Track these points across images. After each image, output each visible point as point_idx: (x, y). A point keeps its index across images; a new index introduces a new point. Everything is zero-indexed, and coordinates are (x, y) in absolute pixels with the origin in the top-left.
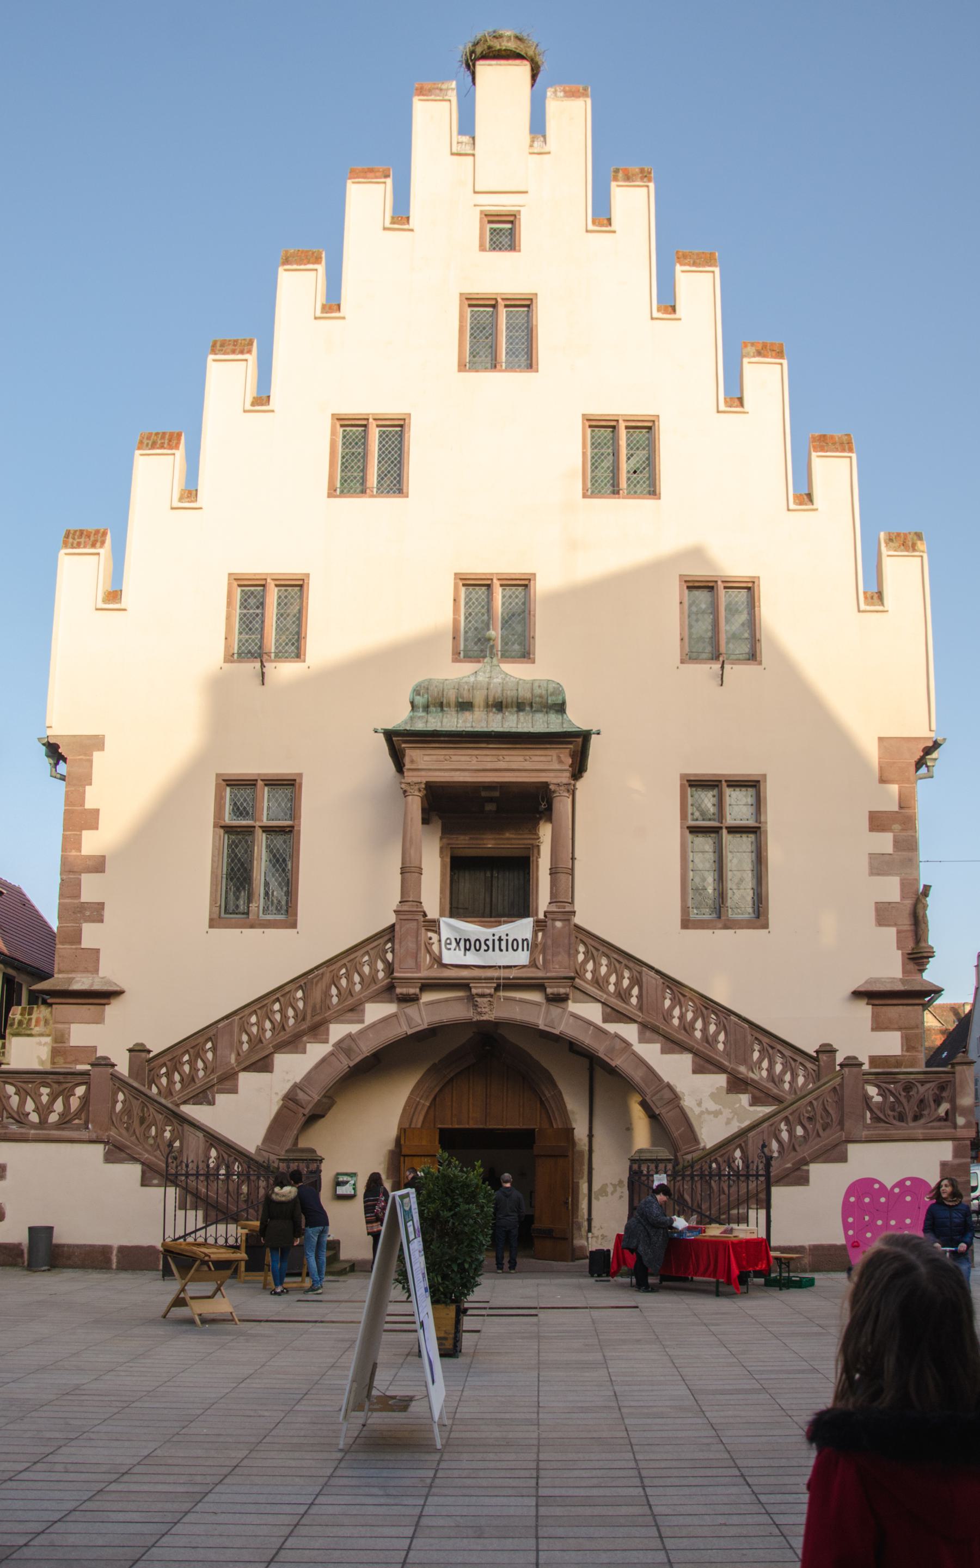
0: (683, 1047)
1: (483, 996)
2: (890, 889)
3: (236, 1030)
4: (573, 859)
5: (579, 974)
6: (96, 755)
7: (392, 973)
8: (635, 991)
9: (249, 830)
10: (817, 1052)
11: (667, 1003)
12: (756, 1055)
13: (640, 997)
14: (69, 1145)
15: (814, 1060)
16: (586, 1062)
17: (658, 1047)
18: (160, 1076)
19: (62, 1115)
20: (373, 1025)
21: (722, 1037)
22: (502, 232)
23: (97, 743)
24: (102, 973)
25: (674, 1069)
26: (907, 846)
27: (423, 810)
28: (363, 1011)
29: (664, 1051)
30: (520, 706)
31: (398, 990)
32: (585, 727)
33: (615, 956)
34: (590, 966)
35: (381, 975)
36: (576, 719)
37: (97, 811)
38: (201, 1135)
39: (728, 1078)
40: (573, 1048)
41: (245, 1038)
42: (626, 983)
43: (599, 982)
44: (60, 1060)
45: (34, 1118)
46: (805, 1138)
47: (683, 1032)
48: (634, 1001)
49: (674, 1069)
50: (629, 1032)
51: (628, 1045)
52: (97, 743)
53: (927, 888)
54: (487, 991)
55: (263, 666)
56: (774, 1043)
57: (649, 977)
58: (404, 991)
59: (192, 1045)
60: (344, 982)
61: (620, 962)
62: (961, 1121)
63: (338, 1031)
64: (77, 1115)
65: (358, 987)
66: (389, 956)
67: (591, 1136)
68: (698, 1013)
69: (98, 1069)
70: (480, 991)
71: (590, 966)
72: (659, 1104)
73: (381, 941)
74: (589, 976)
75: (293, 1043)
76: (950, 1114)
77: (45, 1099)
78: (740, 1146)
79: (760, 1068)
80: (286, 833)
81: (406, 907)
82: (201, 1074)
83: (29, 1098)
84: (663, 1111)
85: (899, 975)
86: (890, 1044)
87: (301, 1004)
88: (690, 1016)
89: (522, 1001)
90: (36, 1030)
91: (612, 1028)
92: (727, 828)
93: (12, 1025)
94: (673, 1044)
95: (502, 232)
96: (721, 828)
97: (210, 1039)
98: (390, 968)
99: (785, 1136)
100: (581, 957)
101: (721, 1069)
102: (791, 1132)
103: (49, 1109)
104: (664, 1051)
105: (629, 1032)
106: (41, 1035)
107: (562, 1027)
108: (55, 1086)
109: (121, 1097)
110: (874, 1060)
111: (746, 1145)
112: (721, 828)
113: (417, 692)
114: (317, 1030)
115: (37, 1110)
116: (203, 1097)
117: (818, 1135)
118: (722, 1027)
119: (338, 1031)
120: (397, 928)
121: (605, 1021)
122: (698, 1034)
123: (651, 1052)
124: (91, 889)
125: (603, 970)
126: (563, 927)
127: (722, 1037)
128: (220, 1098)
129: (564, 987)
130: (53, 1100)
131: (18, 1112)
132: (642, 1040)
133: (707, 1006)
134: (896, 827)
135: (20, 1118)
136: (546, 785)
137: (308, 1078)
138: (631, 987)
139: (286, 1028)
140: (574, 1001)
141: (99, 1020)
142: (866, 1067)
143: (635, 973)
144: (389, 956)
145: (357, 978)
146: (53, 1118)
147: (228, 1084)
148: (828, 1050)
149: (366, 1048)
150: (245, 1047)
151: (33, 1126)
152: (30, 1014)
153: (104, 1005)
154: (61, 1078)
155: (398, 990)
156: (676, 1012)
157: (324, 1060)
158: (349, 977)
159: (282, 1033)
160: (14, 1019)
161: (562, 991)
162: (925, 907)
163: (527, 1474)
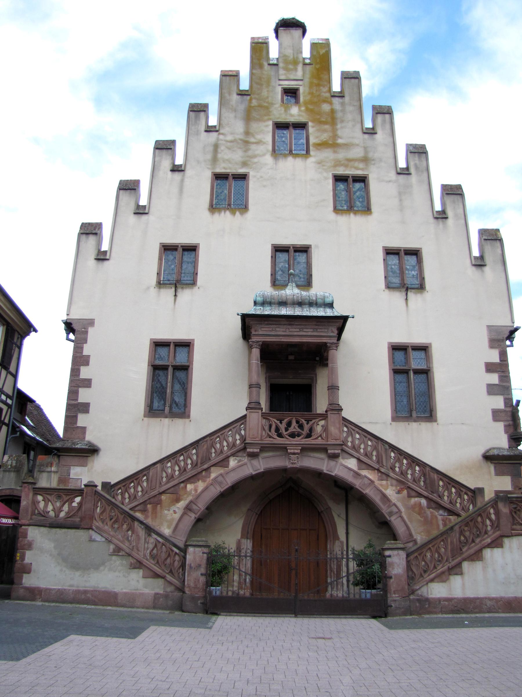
1: (294, 454)
2: (499, 402)
5: (344, 444)
6: (91, 330)
7: (245, 440)
14: (506, 287)
18: (117, 495)
23: (91, 322)
31: (248, 450)
32: (345, 314)
34: (350, 439)
35: (238, 442)
36: (338, 311)
37: (89, 356)
41: (164, 475)
52: (91, 322)
54: (296, 451)
58: (251, 450)
66: (243, 432)
70: (292, 451)
74: (349, 444)
83: (50, 503)
87: (195, 457)
91: (364, 473)
92: (413, 370)
96: (410, 370)
112: (410, 370)
115: (54, 510)
119: (214, 473)
121: (359, 469)
131: (43, 511)
136: (326, 344)
139: (187, 469)
140: (343, 458)
141: (84, 465)
143: (374, 443)
144: (243, 432)
145: (225, 444)
153: (87, 456)
155: (248, 450)
158: (221, 443)
161: (336, 451)
162: (518, 411)
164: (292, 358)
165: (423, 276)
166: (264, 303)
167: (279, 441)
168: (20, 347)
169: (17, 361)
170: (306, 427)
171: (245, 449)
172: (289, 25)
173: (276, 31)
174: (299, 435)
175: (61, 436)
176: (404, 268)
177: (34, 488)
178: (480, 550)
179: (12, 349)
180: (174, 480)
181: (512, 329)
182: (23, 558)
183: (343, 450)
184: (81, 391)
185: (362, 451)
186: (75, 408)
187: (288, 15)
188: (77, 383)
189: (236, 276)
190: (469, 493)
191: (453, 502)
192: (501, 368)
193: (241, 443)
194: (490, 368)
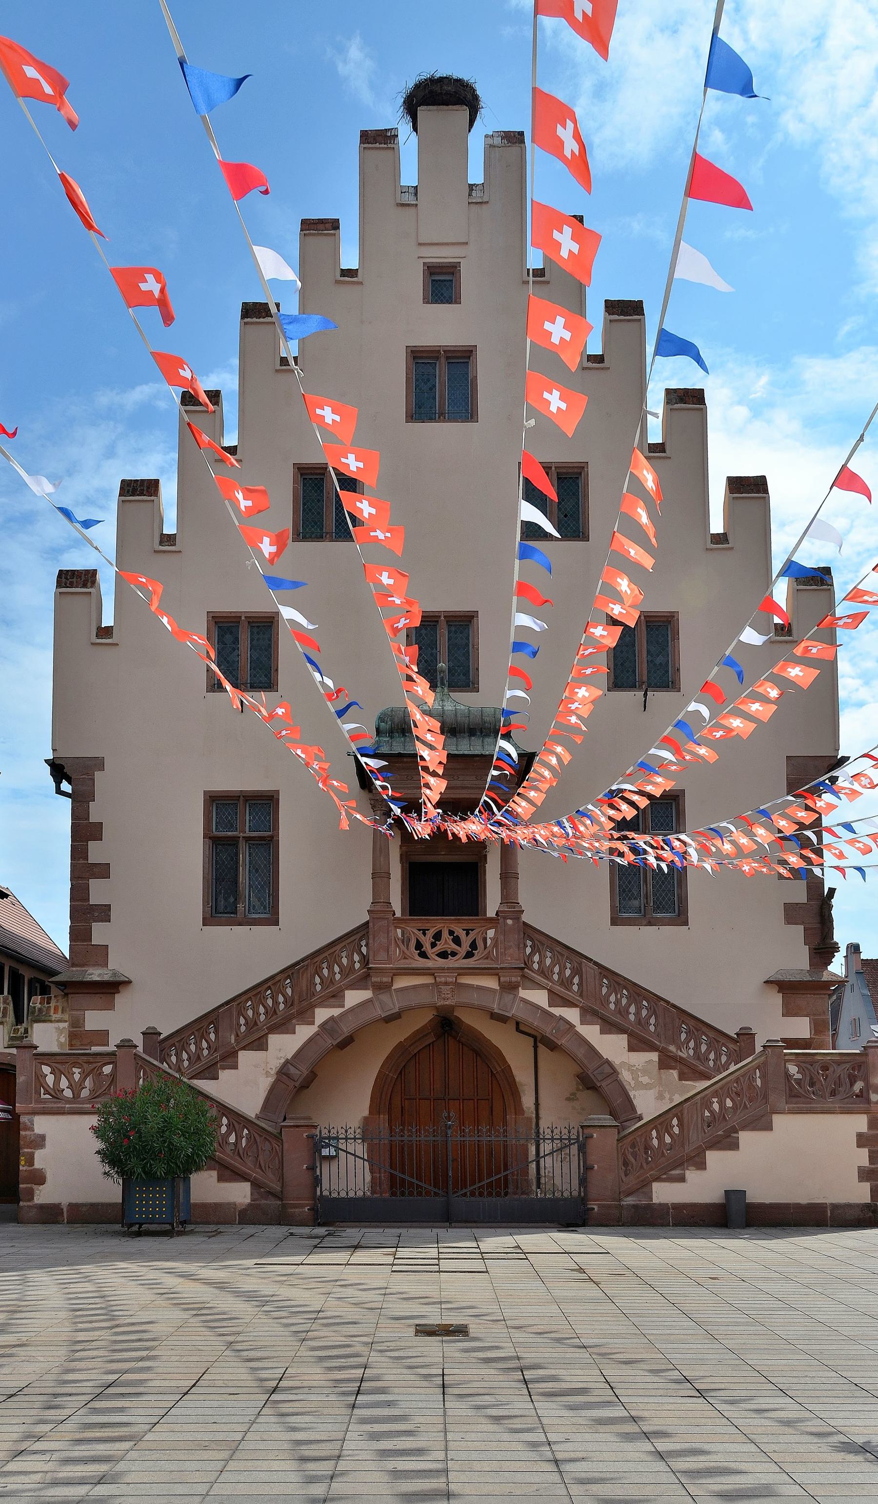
0: (621, 1030)
1: (446, 984)
3: (235, 1013)
5: (528, 964)
7: (368, 964)
8: (576, 980)
9: (233, 842)
10: (737, 1034)
11: (604, 990)
12: (683, 1036)
13: (580, 985)
17: (597, 1028)
20: (352, 1010)
21: (652, 1020)
22: (442, 284)
23: (98, 763)
24: (111, 966)
25: (612, 1047)
29: (602, 1032)
31: (374, 979)
33: (558, 949)
34: (536, 958)
35: (357, 966)
39: (659, 1056)
41: (242, 1021)
42: (568, 972)
43: (545, 972)
44: (76, 1042)
45: (68, 1093)
46: (735, 1108)
47: (619, 1016)
48: (575, 988)
49: (612, 1047)
50: (572, 1015)
51: (572, 1026)
52: (98, 763)
56: (699, 1027)
57: (588, 968)
60: (325, 972)
61: (562, 955)
63: (322, 1014)
67: (537, 1104)
68: (631, 999)
69: (123, 1050)
70: (443, 979)
72: (600, 1078)
74: (536, 966)
75: (284, 1026)
76: (864, 1091)
77: (77, 1077)
78: (676, 1115)
80: (268, 844)
81: (378, 907)
82: (205, 1052)
84: (604, 1084)
85: (807, 967)
88: (624, 1001)
89: (479, 988)
90: (54, 1017)
91: (557, 1011)
93: (33, 1013)
94: (609, 1026)
95: (442, 284)
98: (365, 960)
101: (652, 1048)
102: (721, 1103)
104: (602, 1032)
105: (572, 1015)
106: (58, 1021)
107: (515, 1011)
108: (85, 1065)
111: (682, 1114)
113: (381, 719)
114: (305, 1015)
115: (70, 1087)
117: (745, 1107)
118: (653, 1011)
119: (322, 1014)
120: (371, 924)
122: (632, 1017)
123: (591, 1033)
125: (548, 961)
126: (513, 925)
127: (652, 1020)
128: (224, 1074)
129: (516, 976)
131: (54, 1089)
132: (583, 1023)
133: (638, 992)
135: (56, 1095)
138: (572, 977)
141: (111, 1007)
143: (576, 964)
146: (85, 1093)
150: (243, 1029)
151: (68, 1101)
152: (48, 1003)
154: (91, 1059)
155: (374, 979)
156: (612, 998)
157: (310, 1040)
158: (330, 968)
159: (275, 1017)
160: (34, 1007)
161: (514, 979)
162: (830, 907)
163: (381, 1330)
165: (677, 665)
167: (421, 963)
170: (466, 942)
171: (367, 976)
172: (442, 97)
174: (454, 954)
175: (732, 290)
177: (35, 1055)
180: (258, 1030)
181: (833, 762)
182: (31, 1161)
183: (524, 976)
184: (95, 885)
185: (556, 977)
186: (85, 913)
188: (84, 871)
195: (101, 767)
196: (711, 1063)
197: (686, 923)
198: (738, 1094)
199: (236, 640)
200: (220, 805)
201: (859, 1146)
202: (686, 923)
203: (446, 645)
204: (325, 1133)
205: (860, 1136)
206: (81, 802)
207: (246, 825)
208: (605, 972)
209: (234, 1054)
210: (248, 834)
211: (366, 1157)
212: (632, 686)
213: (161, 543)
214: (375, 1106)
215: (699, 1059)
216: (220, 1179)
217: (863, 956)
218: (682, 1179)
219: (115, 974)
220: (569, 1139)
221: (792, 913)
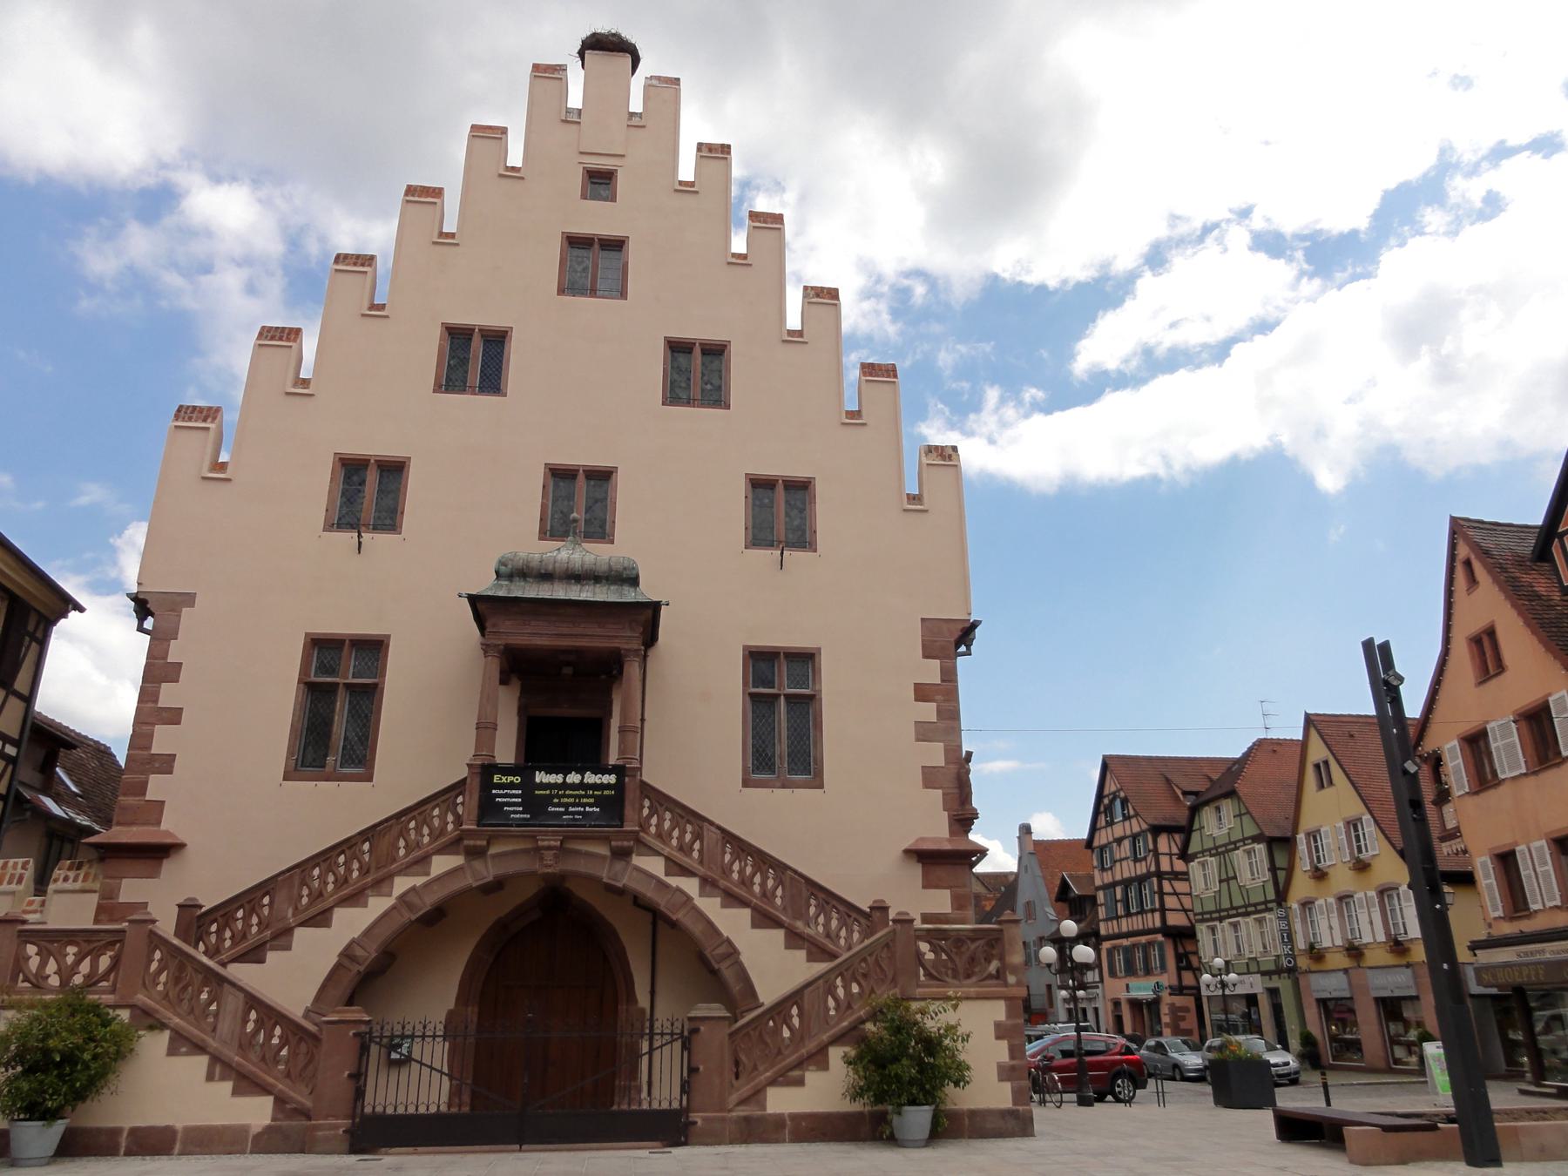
0: (743, 903)
1: (549, 848)
2: (935, 754)
3: (297, 882)
4: (643, 720)
8: (697, 846)
11: (727, 857)
12: (812, 910)
13: (701, 851)
15: (867, 916)
16: (649, 917)
19: (86, 977)
20: (439, 878)
21: (779, 892)
22: (600, 181)
23: (189, 599)
24: (163, 827)
25: (733, 923)
26: (950, 714)
27: (502, 672)
28: (430, 863)
29: (724, 906)
30: (546, 576)
32: (655, 599)
34: (654, 820)
35: (450, 827)
36: (648, 591)
38: (241, 996)
40: (638, 902)
41: (305, 891)
42: (688, 837)
43: (662, 836)
46: (860, 994)
48: (696, 854)
49: (733, 923)
50: (690, 886)
51: (689, 899)
52: (189, 599)
53: (969, 754)
55: (360, 536)
56: (829, 899)
58: (472, 843)
59: (249, 899)
62: (1012, 979)
63: (402, 884)
64: (105, 977)
65: (426, 840)
68: (757, 868)
71: (654, 820)
73: (453, 794)
74: (653, 830)
75: (355, 898)
77: (70, 959)
79: (817, 924)
85: (946, 834)
86: (940, 901)
87: (367, 857)
89: (588, 854)
91: (674, 881)
94: (732, 899)
95: (600, 181)
97: (267, 893)
99: (841, 992)
100: (646, 812)
101: (777, 924)
102: (847, 987)
103: (74, 969)
104: (724, 906)
105: (690, 886)
107: (626, 880)
108: (84, 945)
109: (158, 955)
110: (926, 918)
113: (502, 563)
114: (380, 884)
116: (254, 955)
118: (779, 882)
119: (402, 884)
122: (757, 889)
123: (711, 906)
124: (163, 740)
125: (667, 825)
127: (779, 892)
130: (78, 962)
131: (36, 975)
134: (938, 697)
136: (619, 649)
137: (368, 932)
141: (154, 874)
142: (918, 924)
147: (282, 941)
148: (881, 908)
149: (429, 901)
150: (305, 900)
156: (736, 867)
161: (626, 843)
162: (968, 771)
164: (565, 669)
166: (510, 577)
168: (43, 644)
169: (33, 669)
172: (603, 45)
173: (581, 54)
176: (780, 511)
178: (329, 910)
179: (21, 645)
187: (603, 26)
189: (474, 524)
190: (862, 921)
191: (833, 935)
192: (943, 695)
193: (455, 829)
194: (922, 693)
195: (192, 604)
196: (842, 942)
197: (821, 786)
198: (865, 976)
199: (362, 483)
200: (323, 648)
201: (998, 1037)
202: (821, 786)
203: (579, 496)
204: (398, 1031)
205: (998, 1025)
206: (160, 642)
207: (349, 673)
208: (728, 837)
209: (289, 931)
210: (351, 680)
211: (445, 1070)
212: (770, 545)
213: (295, 385)
214: (462, 998)
215: (828, 936)
216: (236, 1092)
217: (1034, 837)
218: (800, 1082)
219: (168, 833)
220: (672, 1034)
221: (930, 777)
